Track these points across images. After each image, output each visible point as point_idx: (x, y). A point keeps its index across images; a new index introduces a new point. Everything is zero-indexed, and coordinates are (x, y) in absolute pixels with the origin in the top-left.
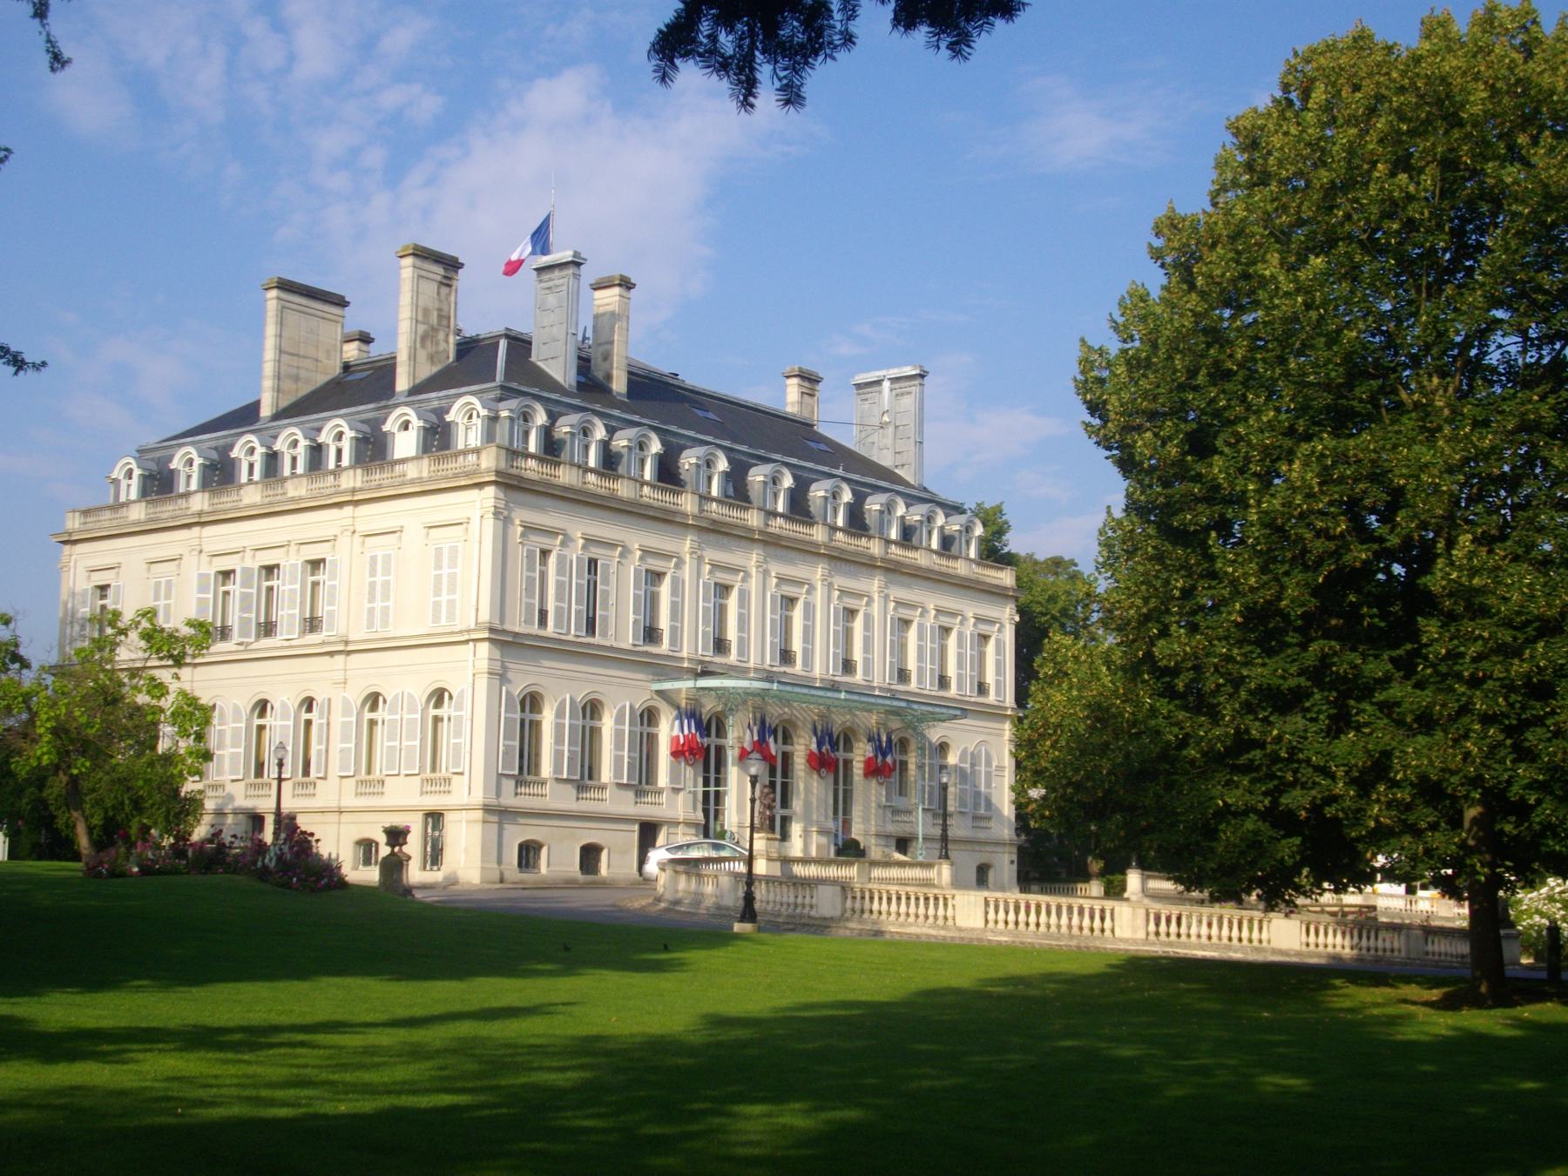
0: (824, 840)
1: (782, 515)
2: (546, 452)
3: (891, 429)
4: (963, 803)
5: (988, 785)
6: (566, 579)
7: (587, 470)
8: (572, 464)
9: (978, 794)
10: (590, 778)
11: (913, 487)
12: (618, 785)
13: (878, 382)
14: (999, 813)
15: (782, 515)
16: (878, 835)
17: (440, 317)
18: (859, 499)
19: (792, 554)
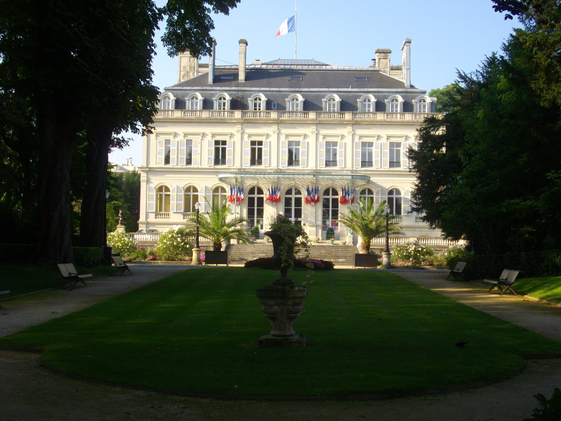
17: (190, 68)
19: (296, 125)
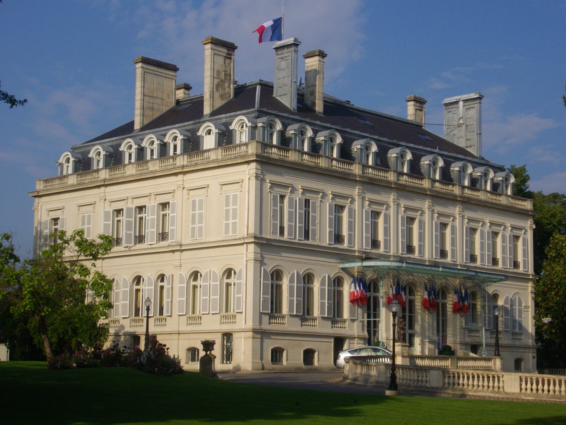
0: (432, 346)
1: (406, 174)
2: (282, 144)
3: (464, 127)
4: (506, 325)
5: (520, 316)
6: (294, 210)
7: (303, 153)
8: (295, 150)
9: (515, 321)
10: (308, 314)
11: (476, 157)
12: (324, 318)
13: (457, 102)
14: (526, 331)
15: (406, 174)
16: (461, 344)
17: (226, 75)
18: (448, 164)
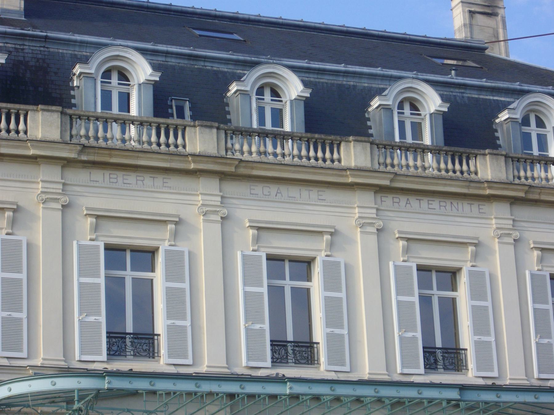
19: (294, 191)
